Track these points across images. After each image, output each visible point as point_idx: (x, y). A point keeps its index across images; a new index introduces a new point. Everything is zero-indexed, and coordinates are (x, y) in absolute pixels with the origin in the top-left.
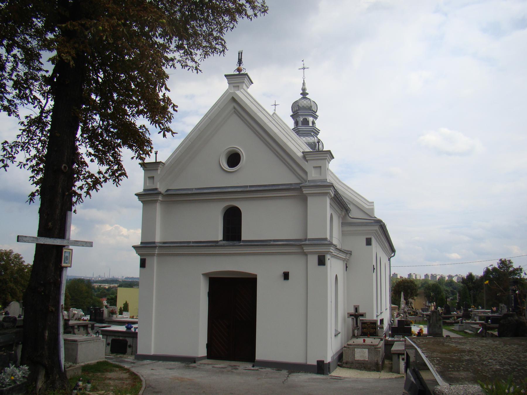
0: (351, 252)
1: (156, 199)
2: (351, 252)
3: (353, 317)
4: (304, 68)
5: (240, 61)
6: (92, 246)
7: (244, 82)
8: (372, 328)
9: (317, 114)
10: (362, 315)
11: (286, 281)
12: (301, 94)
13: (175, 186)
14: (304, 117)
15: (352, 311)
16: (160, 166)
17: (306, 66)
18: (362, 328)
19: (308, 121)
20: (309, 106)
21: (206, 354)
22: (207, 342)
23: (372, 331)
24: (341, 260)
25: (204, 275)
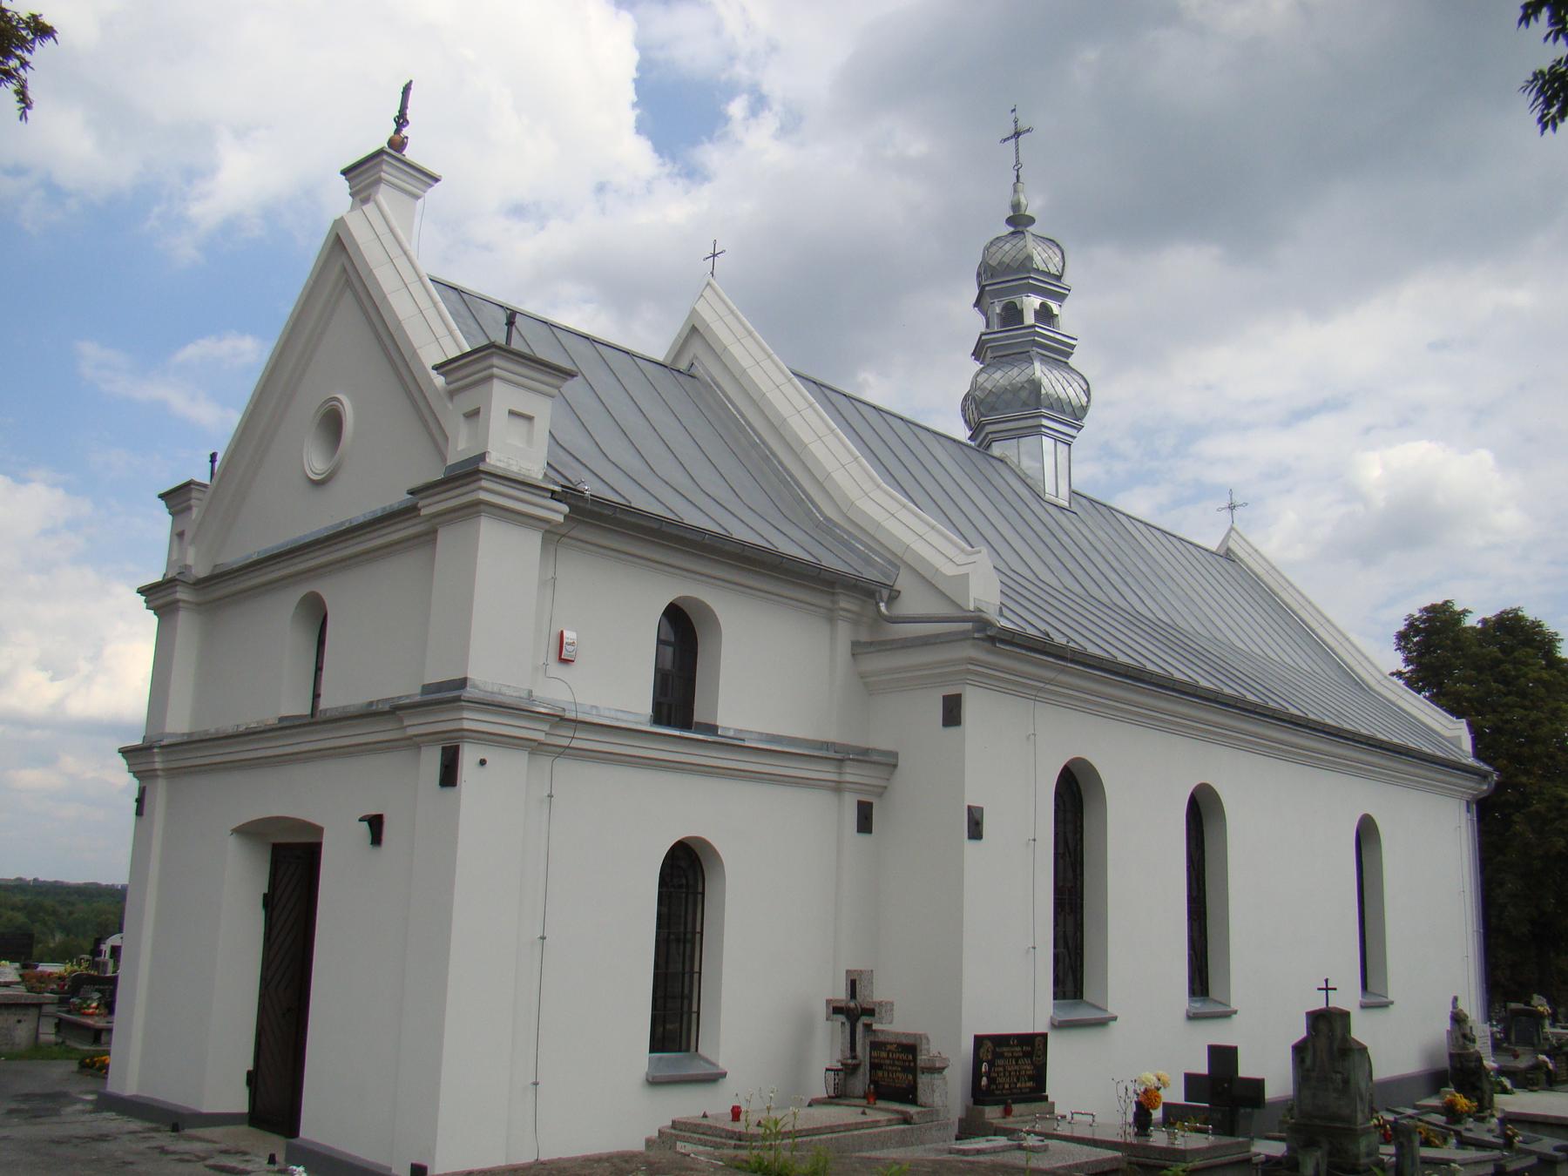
0: (895, 755)
1: (169, 598)
2: (895, 755)
3: (842, 1018)
4: (1017, 134)
5: (401, 120)
6: (970, 837)
7: (379, 181)
8: (905, 1070)
9: (1066, 280)
10: (870, 1012)
11: (377, 849)
12: (1010, 221)
13: (235, 554)
14: (1006, 300)
15: (841, 994)
16: (194, 494)
17: (1023, 125)
18: (874, 1067)
19: (1021, 312)
20: (1021, 257)
21: (245, 1108)
22: (249, 1065)
23: (902, 1079)
24: (821, 787)
25: (249, 832)
